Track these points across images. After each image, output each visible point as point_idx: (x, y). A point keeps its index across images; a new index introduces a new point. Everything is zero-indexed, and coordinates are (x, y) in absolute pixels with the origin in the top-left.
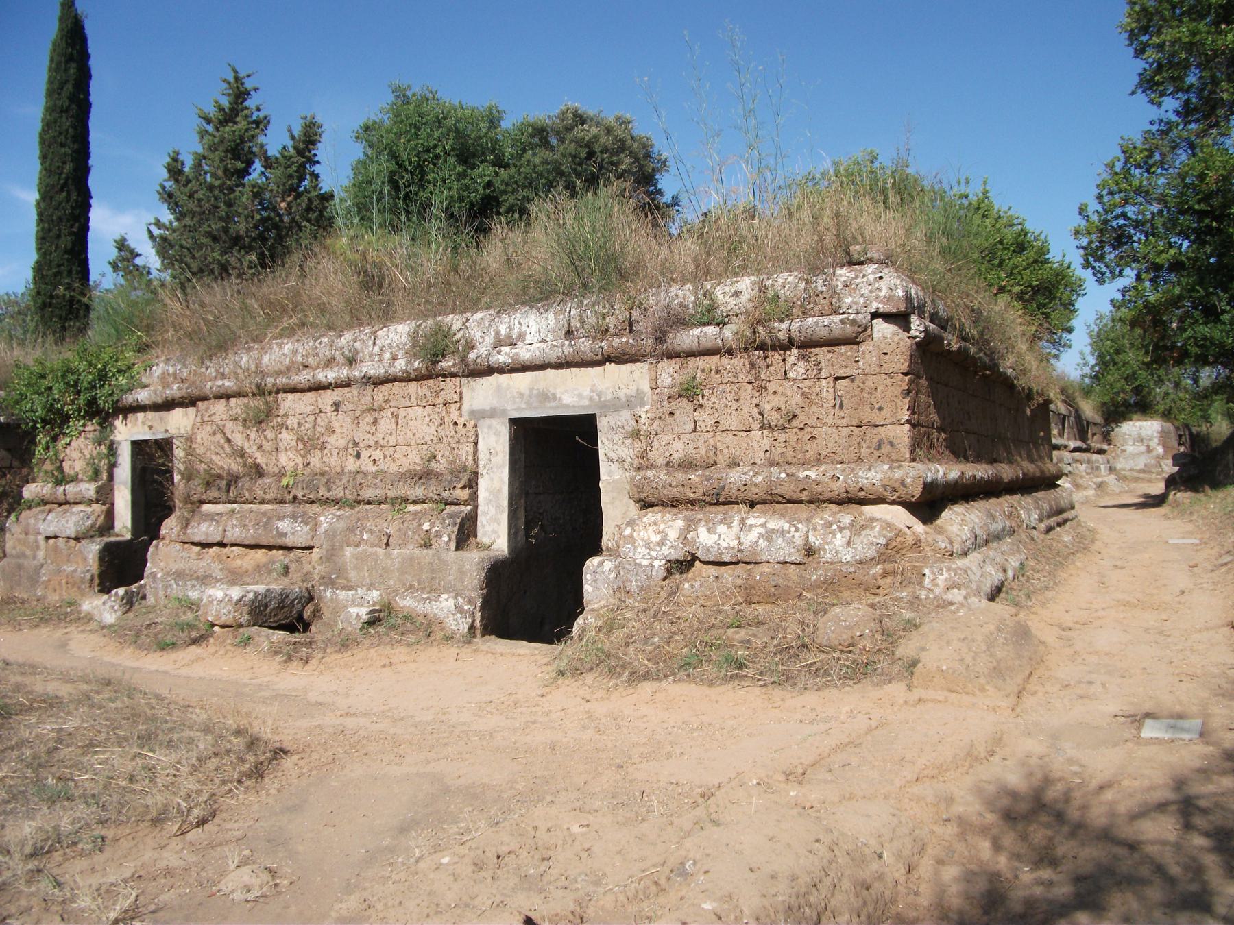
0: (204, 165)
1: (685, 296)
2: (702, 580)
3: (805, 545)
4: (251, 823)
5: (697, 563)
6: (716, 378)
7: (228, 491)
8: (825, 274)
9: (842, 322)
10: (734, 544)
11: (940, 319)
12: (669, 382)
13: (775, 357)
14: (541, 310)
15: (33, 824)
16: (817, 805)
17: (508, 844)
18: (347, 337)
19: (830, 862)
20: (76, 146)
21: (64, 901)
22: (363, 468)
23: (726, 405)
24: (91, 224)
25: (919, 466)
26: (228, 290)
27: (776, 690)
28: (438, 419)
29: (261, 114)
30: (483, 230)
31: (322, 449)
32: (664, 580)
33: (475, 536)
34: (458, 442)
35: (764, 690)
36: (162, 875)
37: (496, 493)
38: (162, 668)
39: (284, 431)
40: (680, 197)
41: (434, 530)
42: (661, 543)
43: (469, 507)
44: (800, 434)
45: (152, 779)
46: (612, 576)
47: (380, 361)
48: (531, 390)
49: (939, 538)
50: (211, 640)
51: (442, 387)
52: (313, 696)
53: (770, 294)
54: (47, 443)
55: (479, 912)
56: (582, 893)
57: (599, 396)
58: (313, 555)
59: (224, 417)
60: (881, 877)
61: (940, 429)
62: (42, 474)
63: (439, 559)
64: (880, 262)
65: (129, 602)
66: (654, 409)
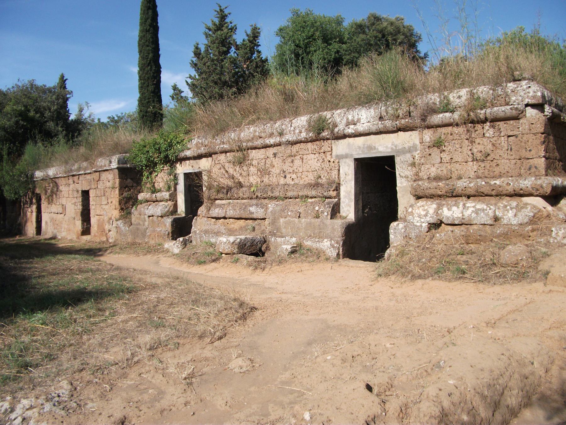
0: (209, 50)
1: (435, 99)
2: (445, 232)
3: (494, 216)
4: (242, 339)
5: (443, 225)
6: (451, 137)
7: (227, 194)
8: (502, 86)
9: (511, 109)
10: (460, 215)
11: (559, 106)
12: (428, 140)
13: (478, 127)
14: (368, 108)
15: (149, 336)
16: (501, 338)
17: (357, 351)
18: (278, 124)
19: (509, 365)
20: (153, 46)
21: (163, 369)
22: (288, 183)
23: (456, 150)
24: (161, 80)
25: (550, 178)
26: (224, 105)
27: (480, 284)
28: (321, 159)
29: (233, 25)
30: (339, 72)
31: (269, 174)
32: (427, 232)
33: (339, 213)
34: (331, 170)
35: (475, 284)
36: (204, 360)
37: (348, 193)
38: (200, 272)
39: (251, 167)
40: (429, 53)
41: (320, 210)
42: (426, 215)
43: (336, 200)
44: (491, 163)
45: (199, 319)
46: (403, 230)
47: (294, 133)
48: (364, 145)
49: (560, 213)
50: (221, 260)
51: (323, 145)
52: (267, 285)
53: (476, 96)
54: (148, 175)
55: (344, 381)
56: (391, 374)
57: (396, 147)
58: (265, 222)
59: (225, 161)
60: (533, 373)
61: (560, 160)
62: (146, 189)
63: (323, 223)
64: (529, 79)
65: (185, 244)
66: (422, 152)
